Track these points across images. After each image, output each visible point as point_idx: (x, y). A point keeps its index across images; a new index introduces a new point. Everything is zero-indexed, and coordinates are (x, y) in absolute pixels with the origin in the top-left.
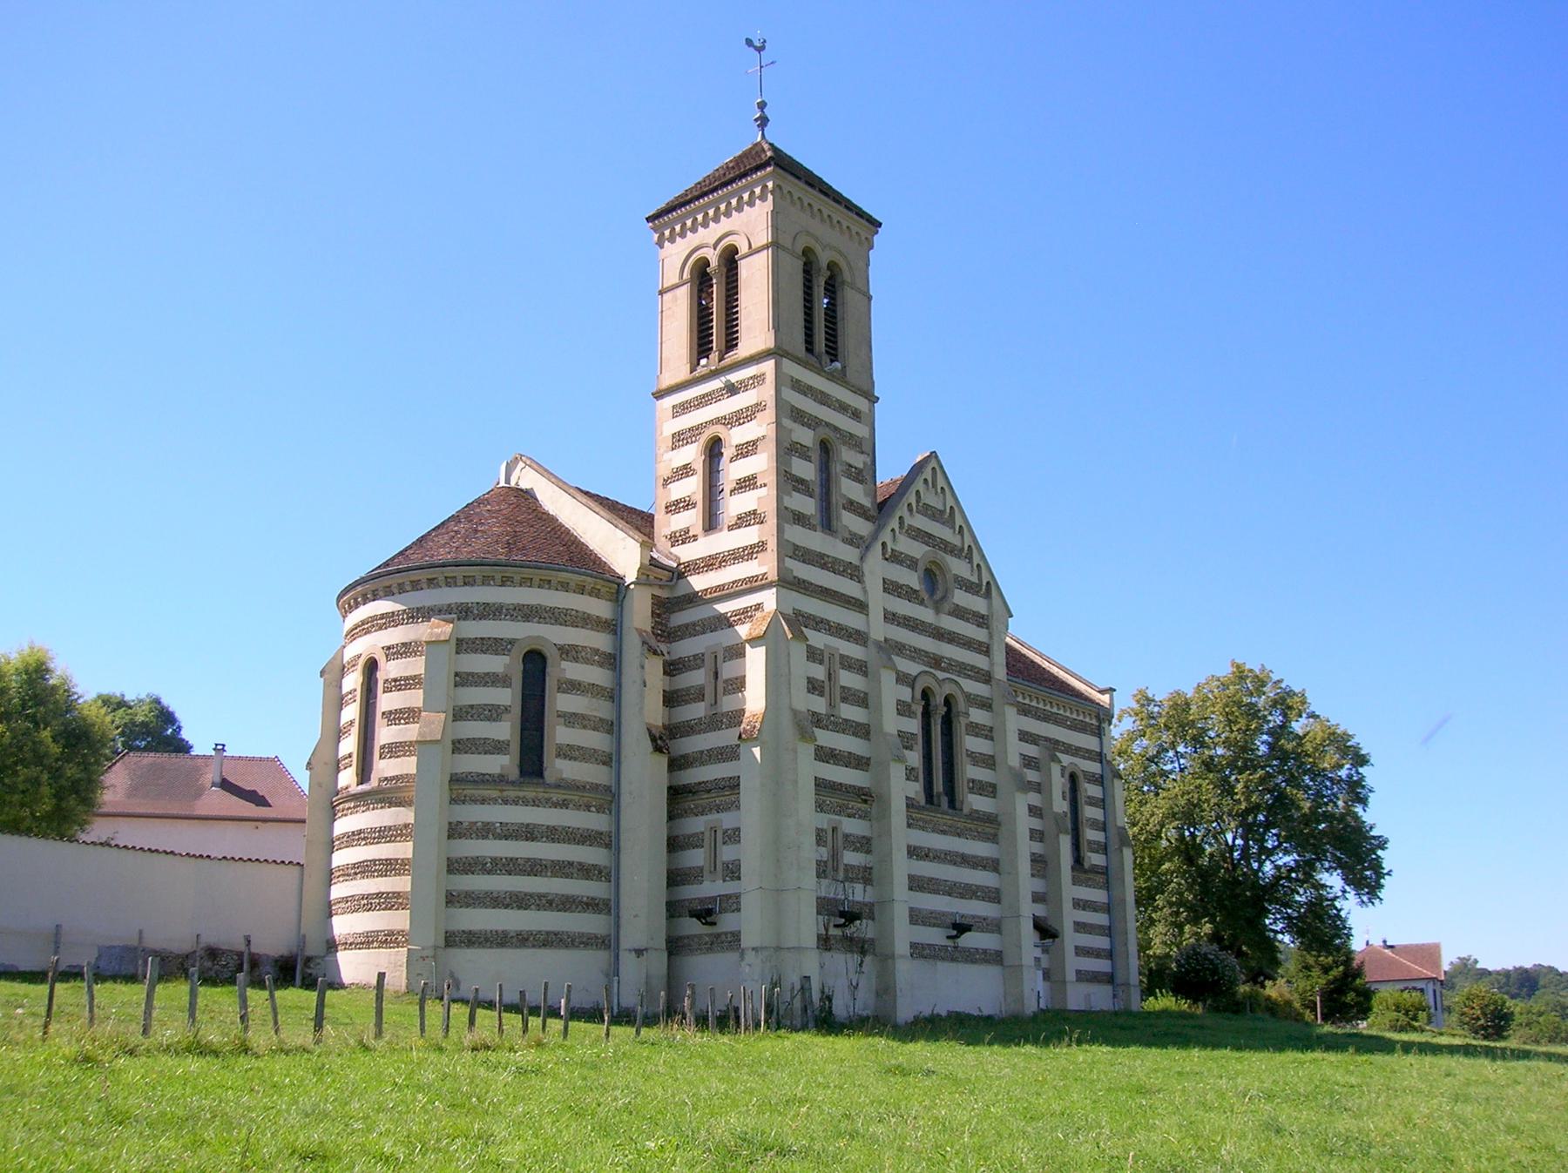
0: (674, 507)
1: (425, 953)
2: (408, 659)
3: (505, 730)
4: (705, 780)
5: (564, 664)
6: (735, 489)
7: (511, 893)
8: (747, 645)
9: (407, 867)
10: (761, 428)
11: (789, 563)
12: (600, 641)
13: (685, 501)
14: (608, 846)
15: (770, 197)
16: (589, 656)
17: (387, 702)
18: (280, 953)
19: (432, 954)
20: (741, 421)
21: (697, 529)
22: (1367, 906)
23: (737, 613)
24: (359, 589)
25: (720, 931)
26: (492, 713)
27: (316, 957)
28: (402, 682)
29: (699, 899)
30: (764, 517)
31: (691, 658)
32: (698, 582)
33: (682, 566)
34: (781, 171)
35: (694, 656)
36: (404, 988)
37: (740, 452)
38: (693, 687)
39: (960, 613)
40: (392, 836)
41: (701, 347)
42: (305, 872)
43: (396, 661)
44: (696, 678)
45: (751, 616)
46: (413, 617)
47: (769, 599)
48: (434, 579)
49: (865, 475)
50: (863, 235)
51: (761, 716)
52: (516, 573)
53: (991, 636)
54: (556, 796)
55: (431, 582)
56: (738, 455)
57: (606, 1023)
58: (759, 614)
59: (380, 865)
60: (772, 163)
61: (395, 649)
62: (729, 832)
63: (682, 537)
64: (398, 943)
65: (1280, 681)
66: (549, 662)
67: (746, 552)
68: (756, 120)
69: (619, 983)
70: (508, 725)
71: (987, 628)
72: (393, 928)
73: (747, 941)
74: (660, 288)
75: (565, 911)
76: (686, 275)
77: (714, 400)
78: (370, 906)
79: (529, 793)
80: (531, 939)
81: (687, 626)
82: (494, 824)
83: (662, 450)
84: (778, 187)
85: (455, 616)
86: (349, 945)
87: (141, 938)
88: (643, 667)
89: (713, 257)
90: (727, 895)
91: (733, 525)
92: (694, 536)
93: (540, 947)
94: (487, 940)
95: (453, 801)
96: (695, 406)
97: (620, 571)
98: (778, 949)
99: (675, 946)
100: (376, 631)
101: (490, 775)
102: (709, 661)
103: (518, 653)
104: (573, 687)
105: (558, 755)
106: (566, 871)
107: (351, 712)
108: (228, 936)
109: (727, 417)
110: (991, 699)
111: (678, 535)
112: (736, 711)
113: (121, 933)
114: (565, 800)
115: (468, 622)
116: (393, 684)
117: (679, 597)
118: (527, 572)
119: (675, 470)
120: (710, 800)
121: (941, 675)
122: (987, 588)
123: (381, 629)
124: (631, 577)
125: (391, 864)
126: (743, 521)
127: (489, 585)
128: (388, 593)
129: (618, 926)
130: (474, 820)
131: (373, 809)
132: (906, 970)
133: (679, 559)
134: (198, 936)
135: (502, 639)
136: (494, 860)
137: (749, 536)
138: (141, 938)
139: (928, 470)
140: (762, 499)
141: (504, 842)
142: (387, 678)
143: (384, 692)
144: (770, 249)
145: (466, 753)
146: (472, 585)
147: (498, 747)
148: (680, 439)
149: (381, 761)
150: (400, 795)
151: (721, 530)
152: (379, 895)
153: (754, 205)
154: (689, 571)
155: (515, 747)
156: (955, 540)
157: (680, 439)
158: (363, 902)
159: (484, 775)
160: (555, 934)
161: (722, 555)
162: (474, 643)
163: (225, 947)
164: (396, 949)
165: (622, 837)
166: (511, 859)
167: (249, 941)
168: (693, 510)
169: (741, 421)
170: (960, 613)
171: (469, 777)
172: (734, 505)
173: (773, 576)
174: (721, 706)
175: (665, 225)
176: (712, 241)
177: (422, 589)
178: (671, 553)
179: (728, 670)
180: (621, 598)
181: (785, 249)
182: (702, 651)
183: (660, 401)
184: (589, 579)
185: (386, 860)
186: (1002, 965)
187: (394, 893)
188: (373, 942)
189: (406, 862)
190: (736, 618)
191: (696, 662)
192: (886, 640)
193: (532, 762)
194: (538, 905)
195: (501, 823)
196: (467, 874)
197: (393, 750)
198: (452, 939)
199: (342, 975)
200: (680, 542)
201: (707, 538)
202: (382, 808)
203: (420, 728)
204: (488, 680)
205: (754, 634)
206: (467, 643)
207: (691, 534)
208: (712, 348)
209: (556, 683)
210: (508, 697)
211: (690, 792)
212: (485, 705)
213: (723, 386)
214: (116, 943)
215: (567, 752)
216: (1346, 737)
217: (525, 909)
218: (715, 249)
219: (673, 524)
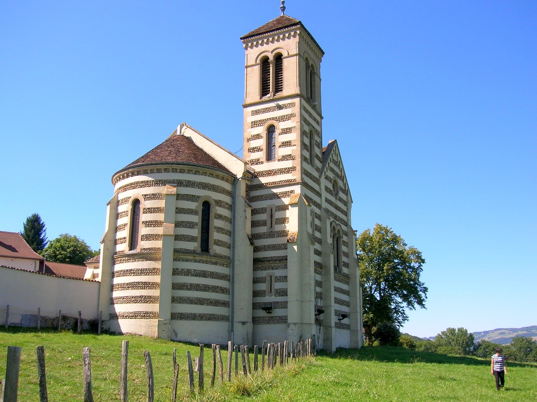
0: (252, 150)
1: (166, 322)
2: (155, 200)
3: (196, 232)
4: (267, 257)
5: (217, 208)
6: (281, 146)
7: (197, 298)
8: (289, 206)
9: (154, 286)
10: (294, 123)
12: (227, 199)
13: (257, 148)
14: (229, 280)
15: (298, 37)
16: (225, 205)
17: (144, 217)
18: (91, 319)
19: (169, 322)
20: (284, 120)
22: (412, 310)
23: (282, 193)
24: (131, 170)
25: (273, 315)
26: (191, 225)
27: (105, 321)
28: (152, 210)
29: (263, 303)
30: (295, 157)
31: (260, 209)
32: (264, 180)
33: (256, 173)
34: (301, 27)
35: (261, 208)
36: (156, 334)
37: (283, 132)
38: (261, 220)
39: (341, 200)
40: (147, 273)
41: (264, 90)
42: (101, 285)
43: (149, 201)
44: (263, 217)
45: (288, 195)
46: (157, 183)
47: (297, 189)
48: (167, 169)
49: (319, 145)
50: (320, 57)
51: (297, 234)
52: (201, 169)
53: (348, 209)
54: (213, 260)
55: (166, 170)
56: (282, 132)
57: (291, 357)
58: (292, 195)
59: (141, 284)
60: (300, 24)
61: (149, 196)
62: (278, 278)
63: (257, 162)
64: (150, 317)
65: (392, 232)
66: (211, 207)
67: (286, 170)
68: (281, 8)
69: (233, 335)
70: (197, 230)
71: (347, 206)
72: (149, 311)
73: (289, 321)
74: (246, 65)
75: (216, 306)
76: (258, 61)
77: (271, 111)
78: (136, 301)
79: (204, 258)
80: (205, 317)
81: (258, 196)
82: (191, 270)
83: (247, 128)
84: (300, 33)
85: (176, 185)
86: (124, 317)
87: (39, 311)
88: (245, 211)
89: (271, 57)
90: (276, 302)
91: (280, 159)
92: (261, 162)
93: (207, 320)
94: (188, 317)
95: (175, 260)
96: (262, 112)
97: (234, 173)
98: (302, 324)
99: (255, 320)
100: (138, 188)
101: (190, 250)
102: (269, 211)
103: (201, 201)
104: (219, 217)
105: (214, 244)
106: (216, 290)
107: (125, 220)
108: (72, 311)
109: (277, 118)
110: (347, 232)
111: (254, 161)
112: (281, 231)
113: (31, 308)
114: (216, 262)
115: (181, 187)
116: (148, 210)
117: (254, 185)
119: (253, 136)
120: (269, 265)
121: (337, 222)
122: (347, 192)
123: (141, 187)
124: (239, 175)
125: (147, 284)
126: (285, 158)
127: (190, 173)
128: (145, 173)
129: (233, 312)
130: (184, 268)
131: (138, 261)
132: (334, 331)
133: (255, 170)
134: (60, 311)
135: (195, 196)
137: (288, 164)
138: (39, 311)
139: (333, 145)
140: (295, 150)
141: (195, 277)
142: (145, 207)
143: (143, 213)
144: (297, 56)
145: (180, 240)
146: (183, 173)
147: (192, 239)
148: (255, 124)
149: (142, 241)
150: (151, 256)
151: (275, 161)
152: (141, 297)
153: (290, 39)
154: (259, 175)
156: (339, 173)
157: (255, 124)
158: (132, 299)
159: (187, 250)
160: (213, 315)
161: (275, 170)
162: (184, 196)
163: (69, 316)
164: (149, 320)
165: (235, 277)
166: (198, 285)
167: (81, 314)
168: (261, 152)
169: (284, 120)
170: (341, 200)
171: (182, 250)
172: (280, 152)
173: (299, 180)
174: (274, 228)
175: (249, 42)
176: (271, 50)
177: (161, 172)
178: (251, 168)
179: (278, 215)
180: (235, 183)
181: (302, 57)
182: (266, 207)
183: (246, 109)
184: (226, 175)
185: (145, 283)
186: (349, 330)
187: (148, 296)
188: (138, 316)
189: (154, 284)
190: (281, 195)
191: (263, 211)
192: (326, 208)
193: (205, 247)
194: (207, 303)
195: (194, 270)
196: (180, 290)
197: (147, 237)
198: (174, 316)
199: (122, 329)
200: (255, 164)
201: (268, 163)
202: (142, 261)
203: (164, 229)
204: (189, 211)
205: (293, 202)
206: (181, 196)
207: (260, 161)
208: (269, 91)
209: (214, 215)
210: (197, 219)
211: (260, 261)
212: (188, 222)
213: (276, 105)
214: (29, 313)
216: (419, 253)
217: (202, 305)
218: (272, 53)
219: (250, 156)
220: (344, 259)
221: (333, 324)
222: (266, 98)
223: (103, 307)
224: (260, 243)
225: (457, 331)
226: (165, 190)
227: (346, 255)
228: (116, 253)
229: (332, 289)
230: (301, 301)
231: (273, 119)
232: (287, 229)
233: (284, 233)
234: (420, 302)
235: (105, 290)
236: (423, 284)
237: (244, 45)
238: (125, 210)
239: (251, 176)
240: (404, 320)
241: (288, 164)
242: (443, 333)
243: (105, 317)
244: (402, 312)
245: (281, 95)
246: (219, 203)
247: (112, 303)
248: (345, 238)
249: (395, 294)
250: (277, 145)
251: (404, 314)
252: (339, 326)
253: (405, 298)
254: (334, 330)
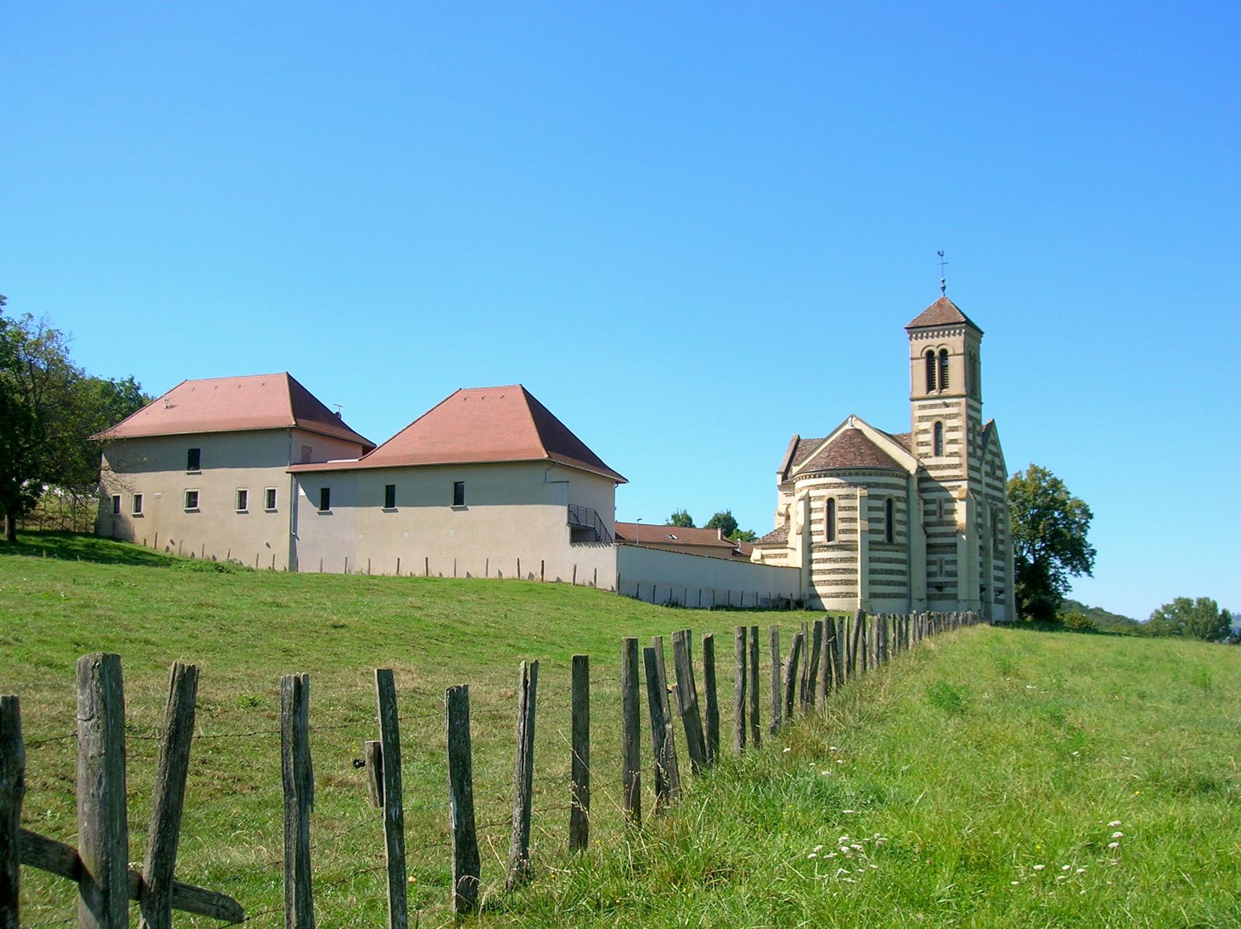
10: (959, 422)
11: (970, 471)
12: (902, 494)
15: (963, 335)
17: (839, 514)
21: (932, 454)
26: (878, 520)
32: (932, 473)
41: (930, 386)
44: (933, 507)
53: (1004, 485)
55: (857, 474)
58: (960, 489)
63: (926, 456)
73: (960, 597)
76: (924, 355)
81: (927, 488)
86: (826, 596)
89: (937, 353)
95: (870, 550)
97: (908, 469)
99: (929, 597)
102: (938, 502)
118: (888, 472)
124: (913, 472)
126: (951, 455)
128: (838, 476)
129: (910, 591)
136: (882, 570)
137: (955, 460)
139: (991, 425)
140: (961, 448)
148: (922, 419)
155: (886, 532)
157: (922, 419)
172: (948, 448)
173: (966, 477)
191: (933, 501)
205: (961, 497)
210: (882, 515)
215: (899, 533)
219: (918, 450)
220: (1000, 537)
221: (992, 601)
222: (934, 393)
223: (805, 590)
224: (931, 530)
225: (1195, 603)
226: (859, 492)
227: (1002, 532)
228: (813, 543)
229: (992, 568)
230: (969, 582)
231: (940, 416)
232: (956, 519)
233: (953, 523)
234: (1087, 568)
235: (805, 574)
236: (1091, 545)
237: (909, 336)
238: (820, 506)
239: (922, 469)
240: (1066, 590)
241: (955, 460)
242: (1166, 608)
243: (807, 597)
244: (1063, 579)
246: (898, 499)
247: (813, 586)
248: (1001, 516)
249: (1054, 556)
250: (944, 442)
251: (1066, 581)
252: (997, 601)
253: (1065, 562)
254: (993, 605)
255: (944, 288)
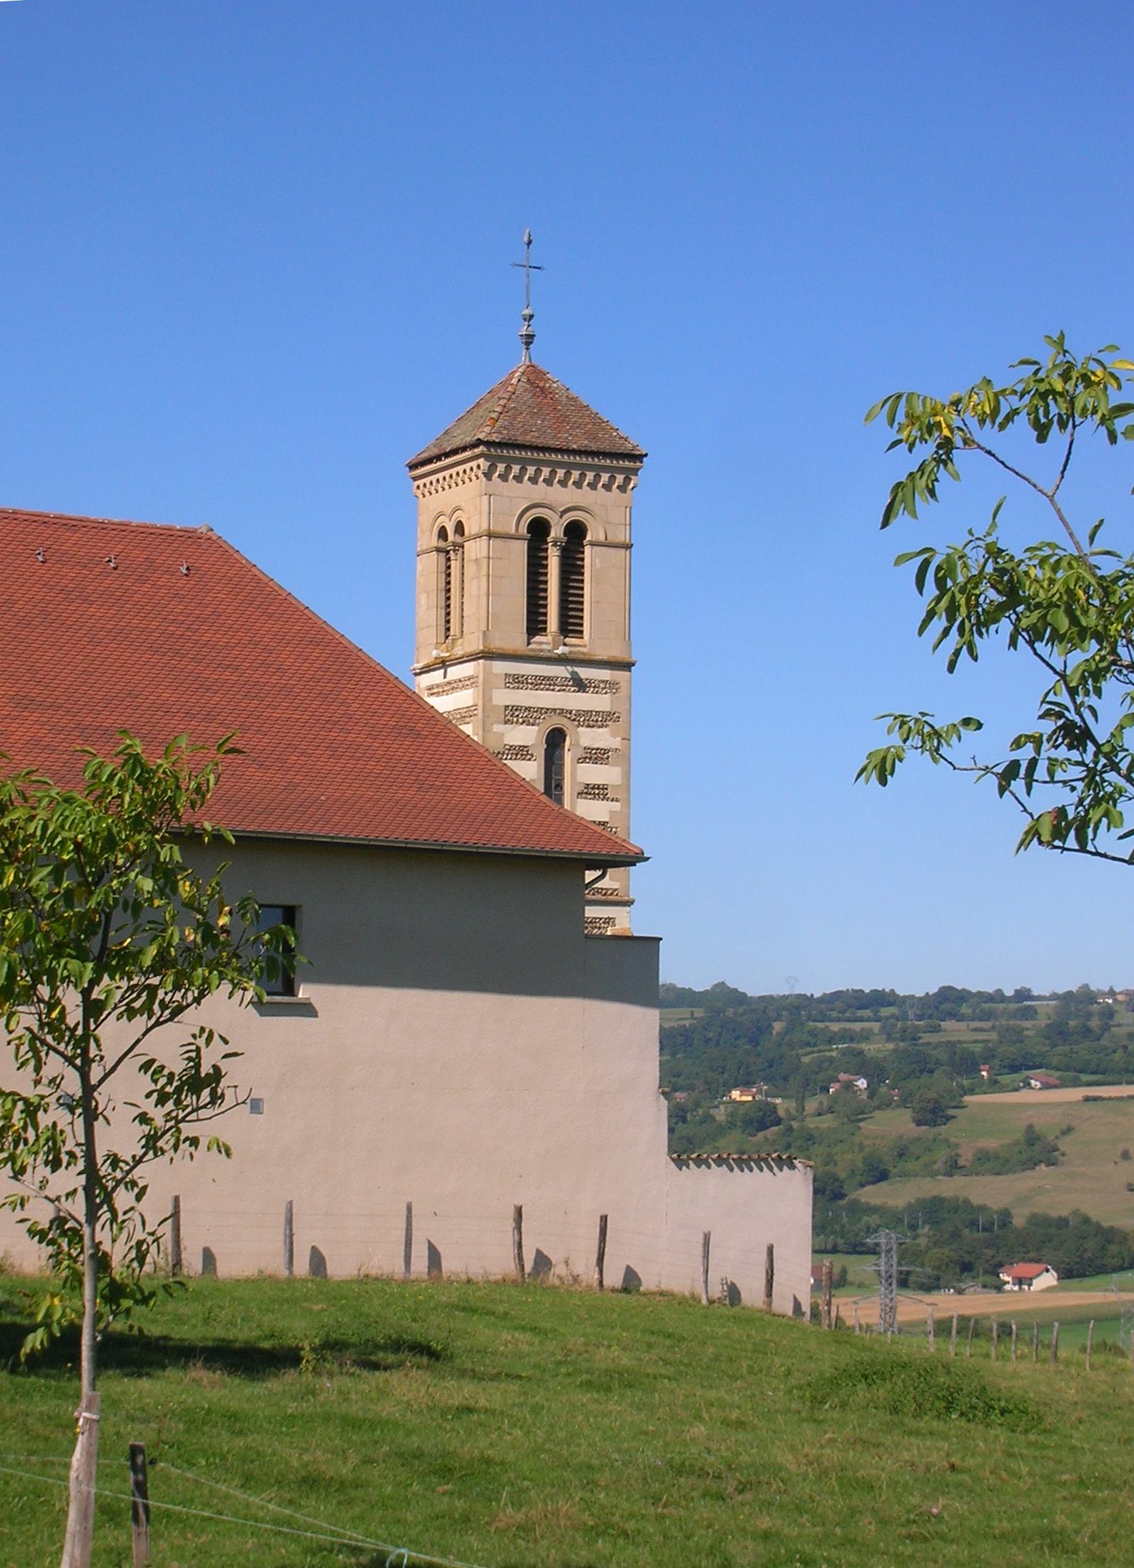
41: (535, 625)
76: (523, 530)
148: (513, 714)
157: (513, 714)
175: (502, 459)
222: (544, 643)
231: (562, 712)
245: (581, 649)
255: (529, 339)
